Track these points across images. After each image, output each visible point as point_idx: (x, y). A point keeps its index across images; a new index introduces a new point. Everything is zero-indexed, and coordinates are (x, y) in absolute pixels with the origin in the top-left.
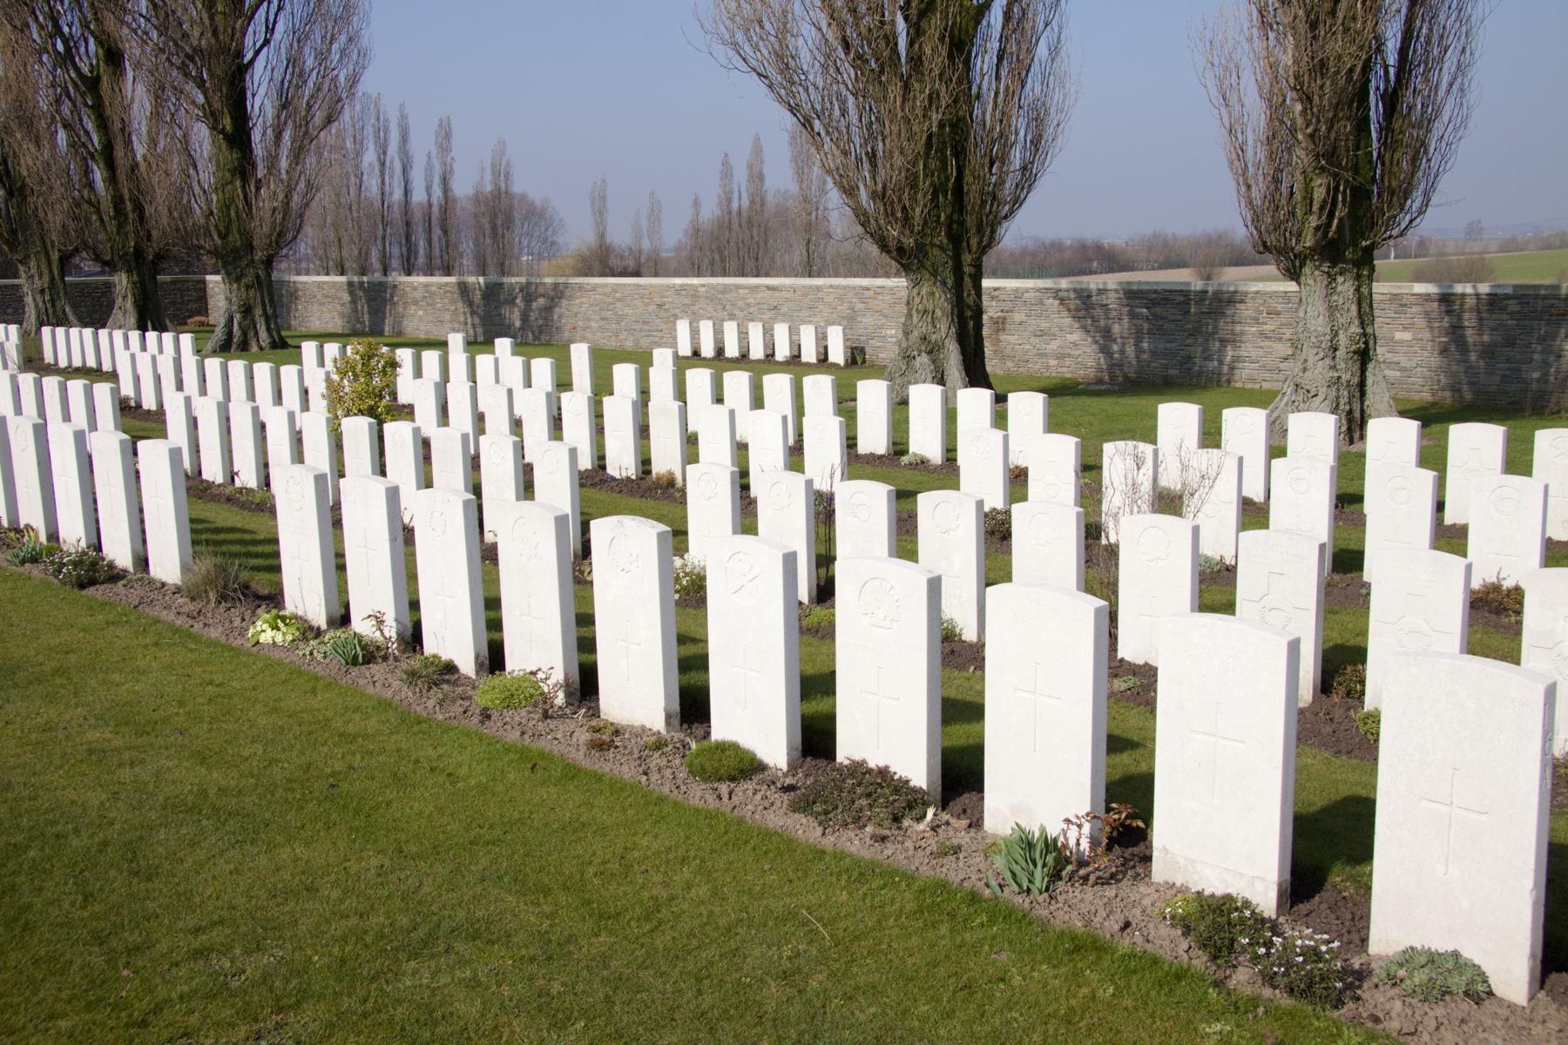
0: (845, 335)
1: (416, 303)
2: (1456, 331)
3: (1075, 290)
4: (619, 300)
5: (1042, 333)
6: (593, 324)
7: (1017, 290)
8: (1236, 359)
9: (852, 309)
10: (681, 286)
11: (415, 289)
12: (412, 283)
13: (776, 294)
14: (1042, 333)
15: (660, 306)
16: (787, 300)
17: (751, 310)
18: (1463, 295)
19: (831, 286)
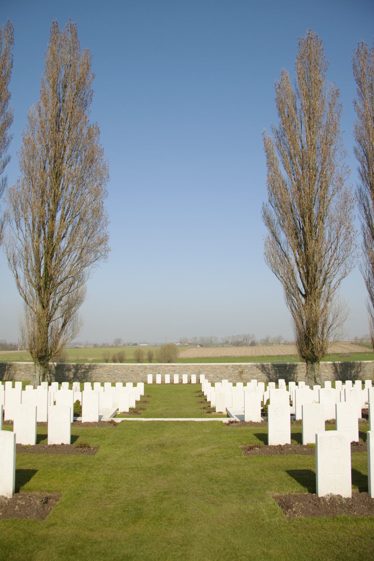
0: (197, 377)
1: (21, 370)
2: (336, 369)
3: (261, 365)
4: (115, 369)
5: (252, 374)
6: (104, 376)
7: (246, 365)
8: (297, 377)
9: (199, 370)
10: (140, 366)
11: (21, 366)
12: (20, 364)
13: (175, 367)
14: (252, 374)
15: (132, 371)
16: (178, 369)
17: (166, 371)
18: (337, 363)
19: (192, 365)
